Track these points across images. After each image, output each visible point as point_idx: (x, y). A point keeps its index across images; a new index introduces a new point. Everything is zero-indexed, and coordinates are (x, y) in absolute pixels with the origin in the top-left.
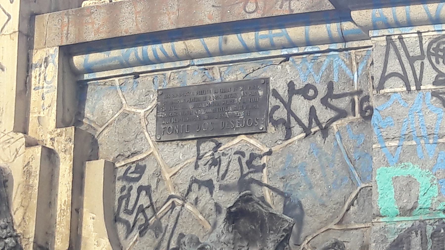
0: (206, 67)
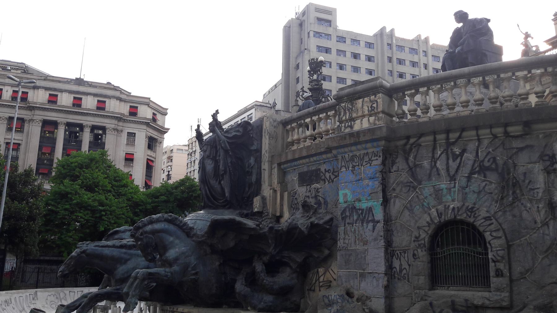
0: (308, 166)
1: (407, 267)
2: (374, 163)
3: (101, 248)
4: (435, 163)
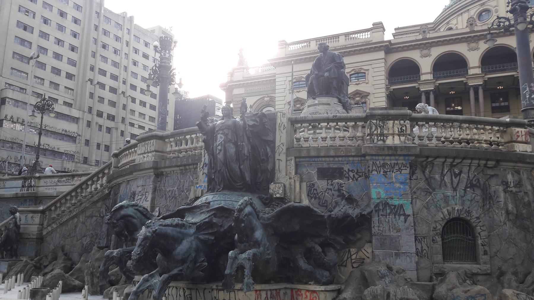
0: (328, 164)
1: (427, 248)
2: (403, 172)
3: (164, 228)
4: (444, 177)
